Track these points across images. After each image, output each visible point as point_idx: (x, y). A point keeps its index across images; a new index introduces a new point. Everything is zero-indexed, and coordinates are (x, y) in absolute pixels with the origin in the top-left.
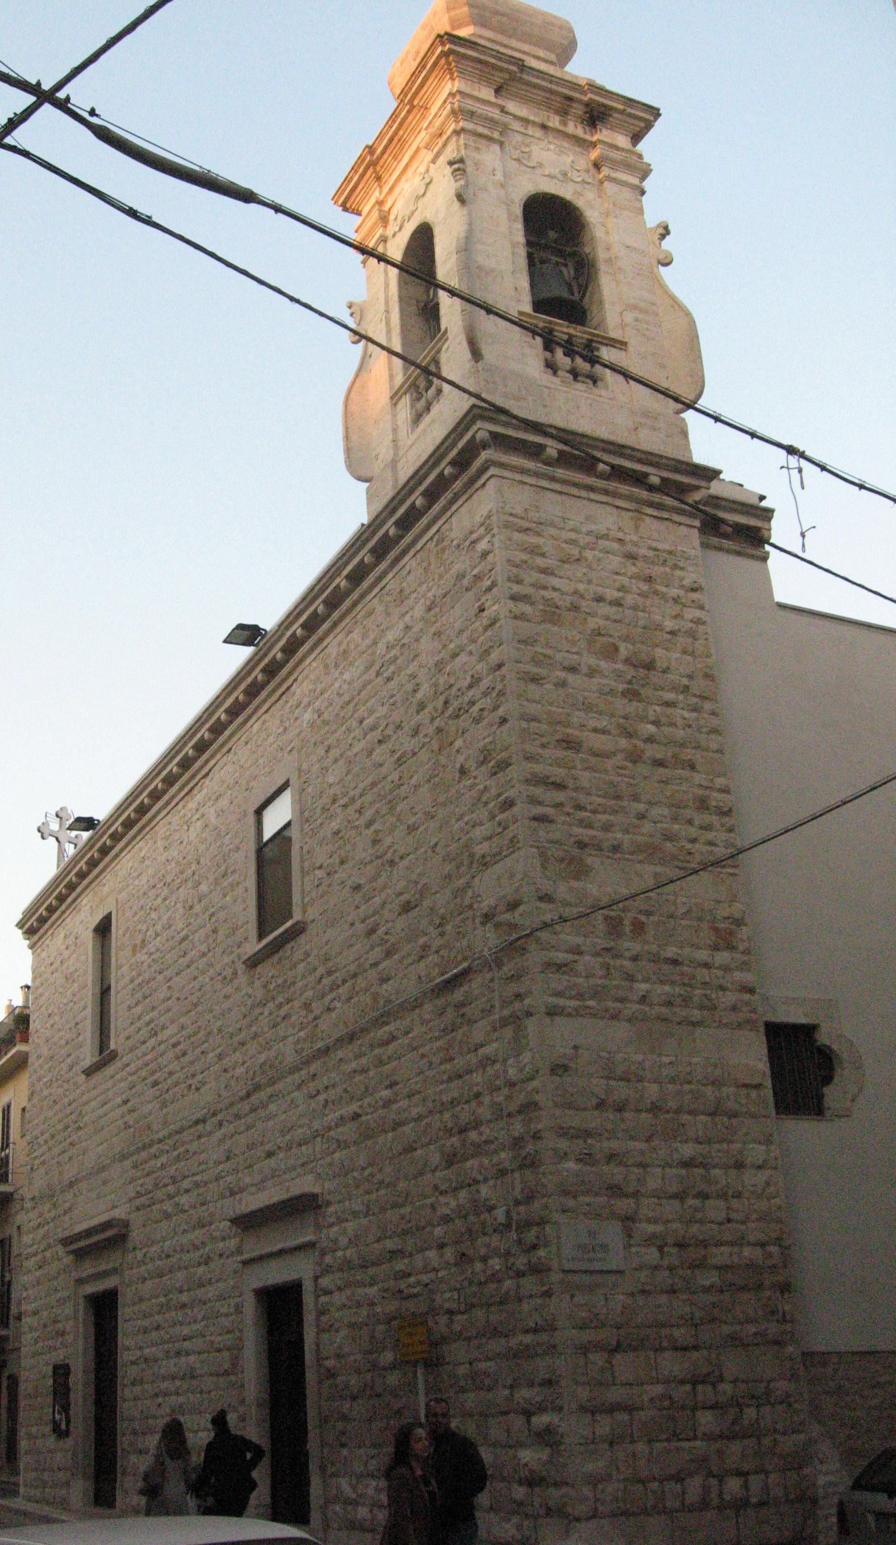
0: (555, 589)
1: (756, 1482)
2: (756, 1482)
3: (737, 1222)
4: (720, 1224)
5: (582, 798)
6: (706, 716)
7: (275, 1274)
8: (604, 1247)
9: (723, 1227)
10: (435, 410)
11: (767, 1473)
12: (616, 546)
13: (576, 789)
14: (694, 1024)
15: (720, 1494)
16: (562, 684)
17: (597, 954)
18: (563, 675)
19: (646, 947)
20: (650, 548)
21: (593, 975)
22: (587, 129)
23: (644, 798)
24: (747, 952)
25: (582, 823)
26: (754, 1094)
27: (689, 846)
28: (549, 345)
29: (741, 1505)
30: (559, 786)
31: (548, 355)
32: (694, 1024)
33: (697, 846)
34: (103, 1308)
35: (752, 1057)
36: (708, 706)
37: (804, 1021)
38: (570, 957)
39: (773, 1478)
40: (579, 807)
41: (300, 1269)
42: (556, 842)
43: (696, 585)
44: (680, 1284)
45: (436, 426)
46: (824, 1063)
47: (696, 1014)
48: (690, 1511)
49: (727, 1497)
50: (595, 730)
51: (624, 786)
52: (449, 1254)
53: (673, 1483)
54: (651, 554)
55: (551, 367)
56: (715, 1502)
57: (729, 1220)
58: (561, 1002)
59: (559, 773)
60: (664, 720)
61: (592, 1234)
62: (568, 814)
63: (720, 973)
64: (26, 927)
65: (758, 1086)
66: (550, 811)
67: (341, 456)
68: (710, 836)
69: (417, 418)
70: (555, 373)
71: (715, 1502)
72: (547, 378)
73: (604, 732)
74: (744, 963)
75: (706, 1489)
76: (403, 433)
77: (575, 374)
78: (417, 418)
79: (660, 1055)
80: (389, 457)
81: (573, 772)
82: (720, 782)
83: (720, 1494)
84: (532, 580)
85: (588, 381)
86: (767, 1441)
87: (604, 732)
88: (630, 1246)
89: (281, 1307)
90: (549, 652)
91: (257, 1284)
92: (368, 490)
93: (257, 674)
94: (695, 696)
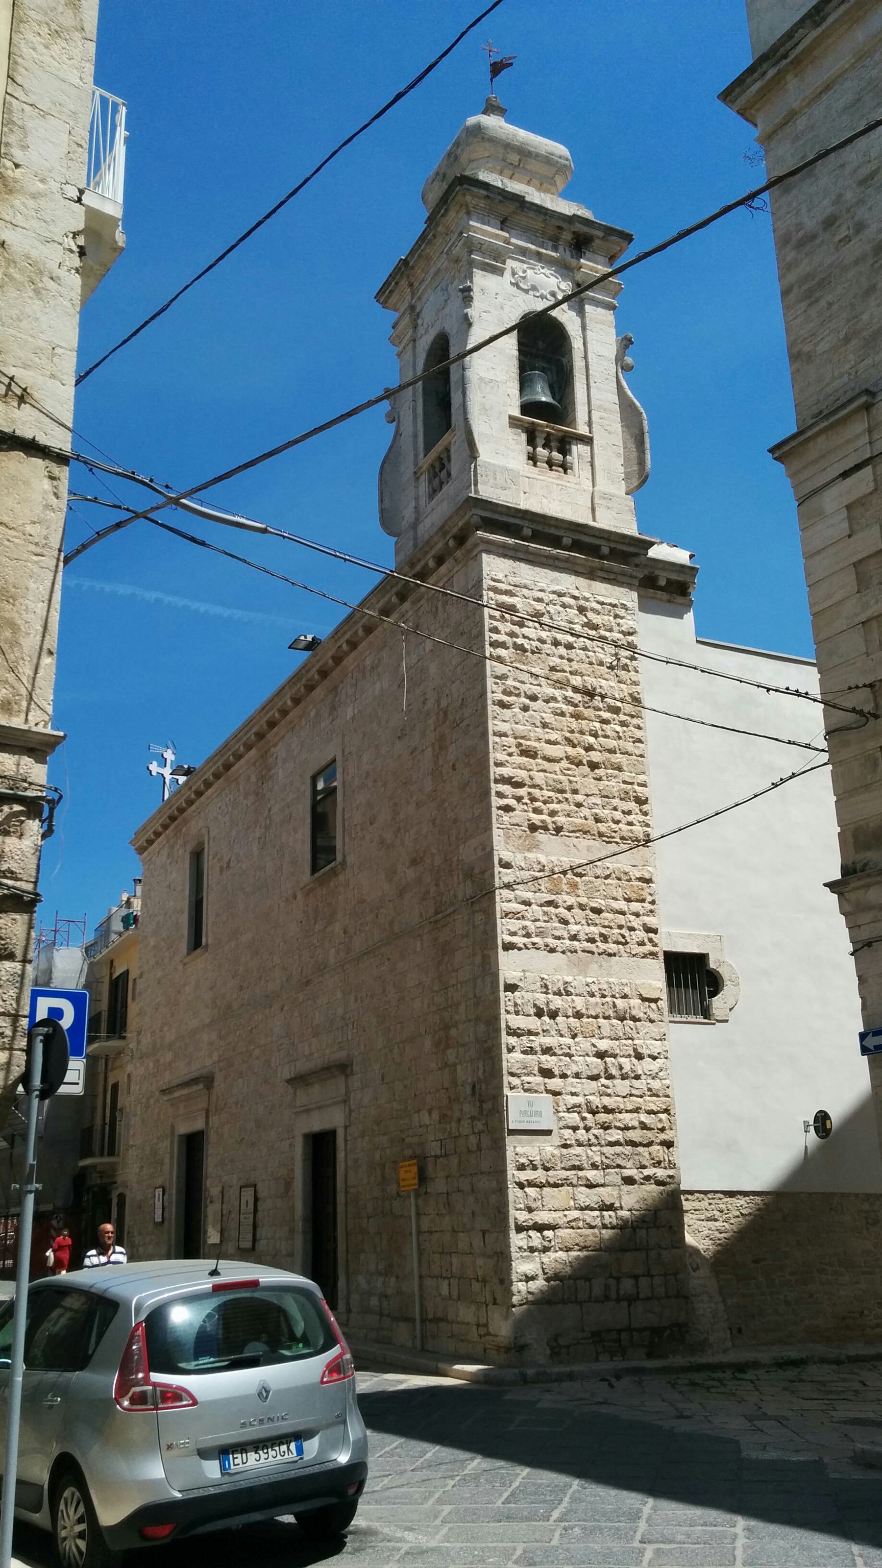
0: (524, 637)
1: (644, 1282)
2: (644, 1282)
3: (637, 1096)
4: (624, 1097)
5: (536, 792)
6: (633, 729)
7: (317, 1124)
8: (539, 1114)
9: (625, 1100)
10: (445, 488)
11: (652, 1276)
12: (572, 602)
13: (534, 786)
14: (610, 955)
15: (618, 1291)
16: (525, 709)
17: (541, 905)
18: (527, 701)
19: (579, 899)
20: (598, 602)
21: (539, 920)
22: (574, 252)
23: (582, 791)
24: (653, 902)
25: (537, 811)
26: (653, 1005)
27: (614, 826)
28: (531, 441)
29: (631, 1300)
30: (519, 785)
31: (530, 449)
32: (610, 955)
33: (620, 825)
34: (193, 1146)
35: (654, 978)
36: (635, 721)
37: (697, 951)
38: (523, 907)
39: (657, 1281)
40: (533, 799)
41: (332, 1119)
42: (518, 825)
43: (631, 631)
44: (594, 1140)
45: (445, 504)
46: (713, 983)
47: (612, 947)
48: (595, 1302)
49: (622, 1292)
50: (549, 742)
51: (567, 783)
52: (435, 1115)
53: (583, 1281)
54: (598, 607)
55: (533, 458)
56: (613, 1295)
57: (631, 1095)
58: (514, 939)
59: (522, 775)
60: (600, 733)
61: (530, 1104)
62: (526, 804)
63: (632, 918)
64: (137, 845)
65: (656, 1001)
66: (512, 802)
67: (377, 515)
68: (630, 818)
69: (433, 492)
70: (535, 465)
71: (613, 1295)
72: (526, 468)
73: (555, 743)
74: (651, 911)
75: (607, 1287)
76: (423, 501)
77: (550, 464)
78: (433, 492)
79: (586, 977)
80: (412, 520)
81: (531, 773)
82: (641, 778)
83: (618, 1291)
84: (507, 630)
85: (560, 469)
86: (653, 1254)
87: (555, 743)
88: (559, 1112)
89: (321, 1146)
90: (517, 685)
91: (306, 1130)
92: (396, 543)
93: (313, 673)
94: (625, 714)
